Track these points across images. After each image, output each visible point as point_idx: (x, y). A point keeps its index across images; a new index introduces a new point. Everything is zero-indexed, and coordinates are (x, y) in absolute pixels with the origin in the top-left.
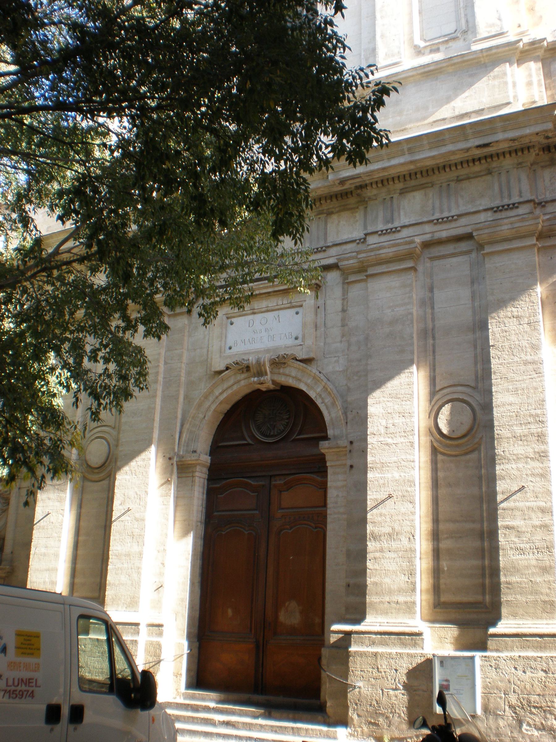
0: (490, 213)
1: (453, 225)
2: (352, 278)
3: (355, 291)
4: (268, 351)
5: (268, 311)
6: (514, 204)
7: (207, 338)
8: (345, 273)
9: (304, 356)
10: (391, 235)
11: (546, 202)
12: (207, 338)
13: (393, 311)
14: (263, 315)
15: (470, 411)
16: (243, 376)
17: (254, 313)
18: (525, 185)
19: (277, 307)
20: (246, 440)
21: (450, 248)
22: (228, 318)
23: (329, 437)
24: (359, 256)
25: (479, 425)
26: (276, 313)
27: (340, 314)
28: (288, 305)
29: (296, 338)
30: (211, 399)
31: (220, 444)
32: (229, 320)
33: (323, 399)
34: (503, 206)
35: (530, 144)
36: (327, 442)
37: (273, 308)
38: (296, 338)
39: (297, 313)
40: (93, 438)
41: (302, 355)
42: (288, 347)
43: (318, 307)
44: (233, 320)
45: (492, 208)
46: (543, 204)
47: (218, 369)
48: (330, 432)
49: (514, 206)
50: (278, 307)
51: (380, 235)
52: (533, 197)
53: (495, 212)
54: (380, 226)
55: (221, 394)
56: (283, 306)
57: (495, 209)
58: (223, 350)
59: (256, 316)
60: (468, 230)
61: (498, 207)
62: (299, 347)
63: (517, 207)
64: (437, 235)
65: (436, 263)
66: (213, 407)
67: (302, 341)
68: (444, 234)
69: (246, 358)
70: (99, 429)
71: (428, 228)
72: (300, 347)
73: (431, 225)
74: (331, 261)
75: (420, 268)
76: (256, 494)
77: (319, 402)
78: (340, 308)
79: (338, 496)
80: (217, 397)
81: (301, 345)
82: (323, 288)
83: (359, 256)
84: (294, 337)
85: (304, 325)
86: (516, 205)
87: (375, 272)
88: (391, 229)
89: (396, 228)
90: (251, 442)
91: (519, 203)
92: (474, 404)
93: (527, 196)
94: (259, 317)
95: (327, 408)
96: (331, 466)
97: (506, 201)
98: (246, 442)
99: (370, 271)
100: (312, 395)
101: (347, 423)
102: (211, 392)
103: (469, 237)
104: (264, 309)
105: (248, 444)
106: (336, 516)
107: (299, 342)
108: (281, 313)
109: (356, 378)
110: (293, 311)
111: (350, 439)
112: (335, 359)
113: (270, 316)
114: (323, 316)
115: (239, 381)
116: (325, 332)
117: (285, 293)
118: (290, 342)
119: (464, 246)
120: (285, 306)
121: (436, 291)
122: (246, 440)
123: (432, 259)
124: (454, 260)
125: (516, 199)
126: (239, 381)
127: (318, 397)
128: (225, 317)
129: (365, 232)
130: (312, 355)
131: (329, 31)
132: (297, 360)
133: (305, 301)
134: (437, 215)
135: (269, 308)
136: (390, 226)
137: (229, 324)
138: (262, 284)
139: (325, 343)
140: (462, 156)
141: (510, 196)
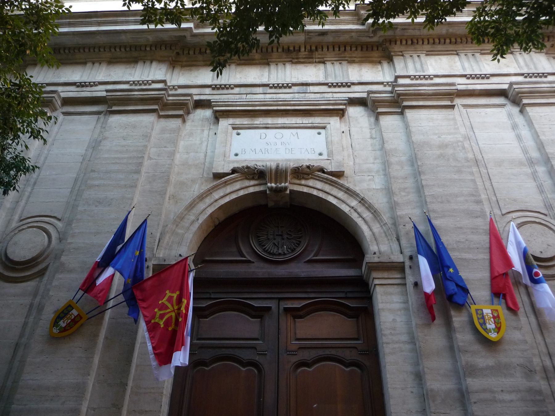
1: (485, 81)
7: (204, 144)
12: (204, 144)
13: (439, 137)
16: (252, 182)
20: (245, 257)
22: (234, 128)
29: (320, 154)
30: (208, 201)
31: (207, 258)
35: (551, 34)
39: (319, 134)
40: (35, 224)
43: (343, 132)
44: (239, 131)
47: (221, 171)
55: (222, 197)
58: (227, 155)
62: (327, 161)
66: (210, 211)
72: (329, 161)
78: (368, 135)
79: (394, 320)
80: (216, 201)
90: (249, 258)
102: (209, 192)
105: (249, 262)
106: (396, 346)
109: (403, 194)
110: (316, 131)
112: (370, 177)
117: (305, 114)
122: (245, 257)
123: (465, 106)
127: (352, 211)
131: (61, 12)
140: (212, 185)
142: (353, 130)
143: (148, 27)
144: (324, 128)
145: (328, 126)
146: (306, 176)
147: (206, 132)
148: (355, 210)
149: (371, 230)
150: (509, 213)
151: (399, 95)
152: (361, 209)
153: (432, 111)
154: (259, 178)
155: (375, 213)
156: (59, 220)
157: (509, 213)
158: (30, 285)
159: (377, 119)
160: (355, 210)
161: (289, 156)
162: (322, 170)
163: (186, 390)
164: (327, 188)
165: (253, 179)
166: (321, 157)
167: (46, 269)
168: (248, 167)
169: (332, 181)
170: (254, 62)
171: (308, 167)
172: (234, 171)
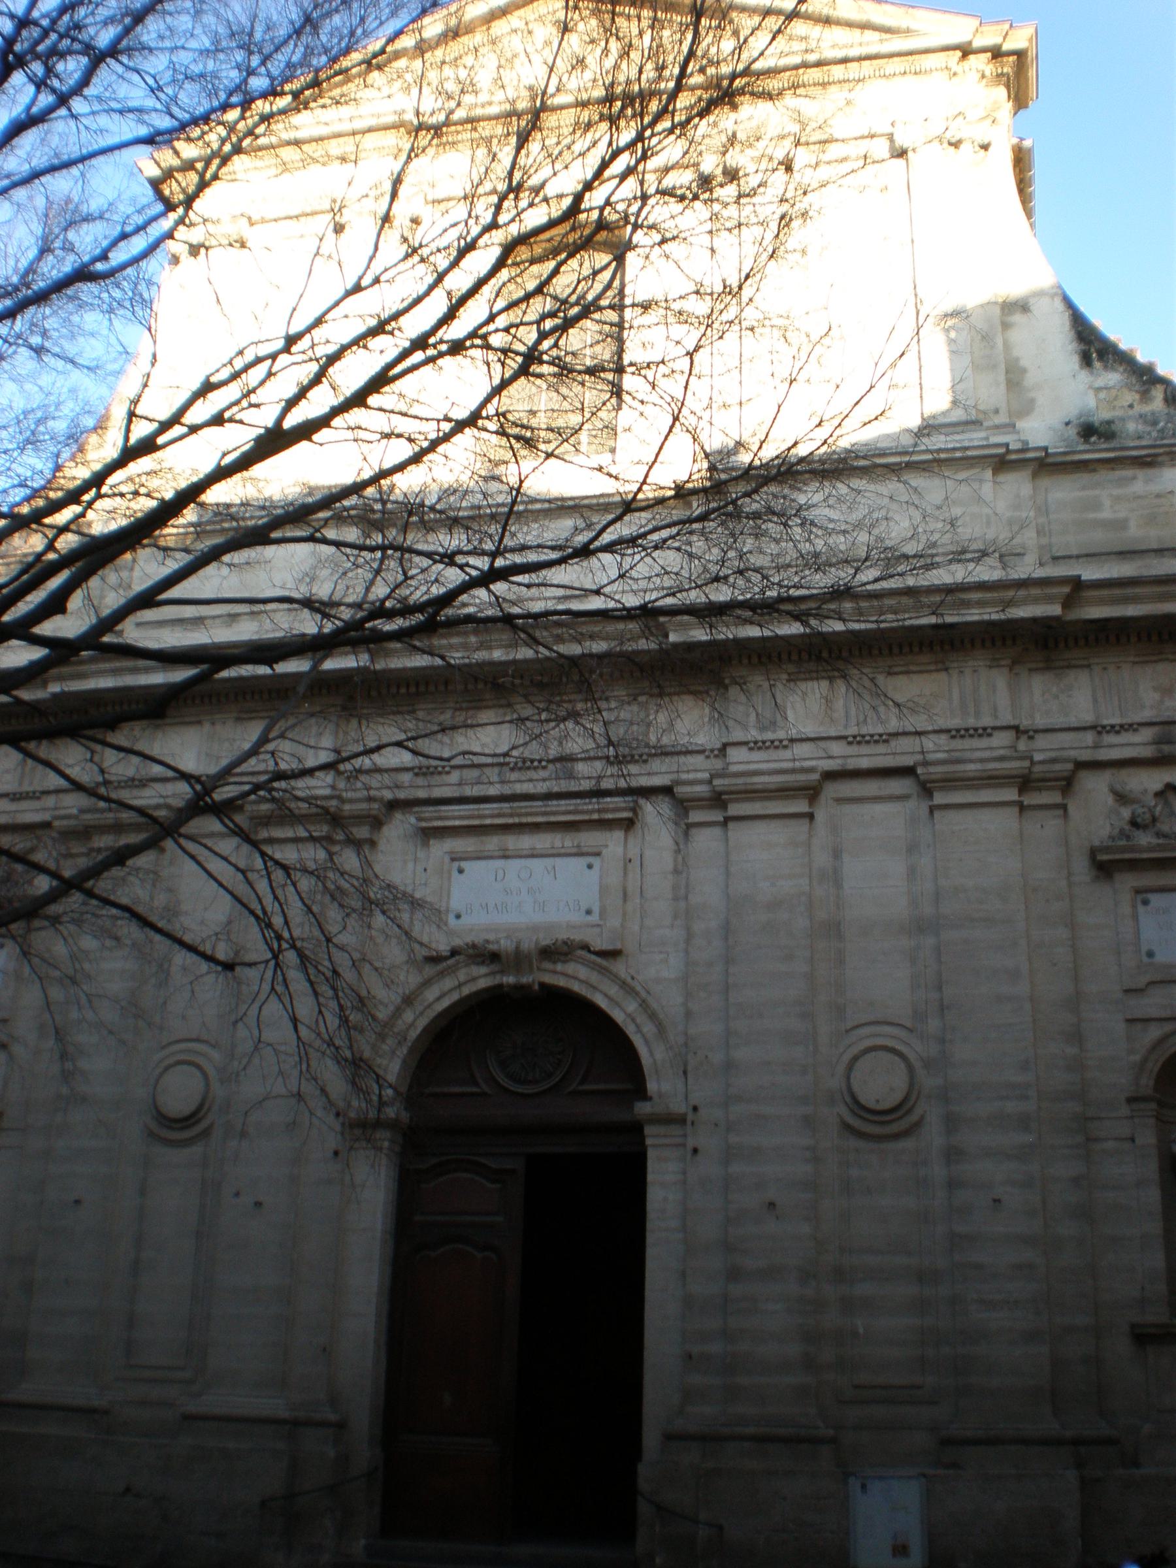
0: (943, 738)
2: (695, 816)
3: (706, 841)
4: (535, 928)
5: (533, 856)
6: (985, 729)
8: (683, 806)
9: (606, 946)
10: (771, 751)
11: (1036, 731)
14: (523, 862)
15: (903, 1065)
16: (483, 970)
17: (506, 857)
18: (1003, 697)
19: (550, 852)
21: (871, 787)
22: (453, 860)
23: (649, 1093)
24: (716, 782)
25: (919, 1093)
26: (549, 862)
27: (670, 877)
28: (574, 850)
29: (589, 912)
32: (456, 864)
33: (637, 1026)
34: (967, 730)
36: (648, 1104)
37: (544, 852)
38: (589, 912)
39: (590, 867)
40: (171, 1060)
41: (599, 944)
42: (574, 927)
44: (464, 864)
45: (949, 731)
46: (1031, 733)
48: (652, 1086)
49: (985, 732)
50: (554, 851)
51: (751, 749)
52: (1016, 722)
53: (953, 737)
54: (754, 734)
55: (438, 999)
56: (563, 851)
57: (954, 733)
59: (510, 862)
60: (908, 761)
61: (958, 731)
63: (990, 735)
64: (852, 764)
65: (848, 809)
67: (601, 919)
68: (865, 763)
69: (491, 937)
70: (183, 1046)
71: (837, 748)
72: (597, 930)
73: (843, 743)
74: (657, 781)
75: (820, 816)
76: (498, 1186)
77: (630, 1030)
78: (671, 867)
81: (598, 925)
82: (638, 825)
83: (716, 782)
84: (583, 909)
85: (604, 890)
86: (989, 731)
87: (742, 813)
88: (772, 742)
89: (781, 741)
90: (486, 1089)
91: (994, 728)
92: (912, 1056)
93: (1006, 718)
94: (514, 865)
95: (646, 1041)
96: (654, 1146)
97: (971, 722)
98: (475, 1089)
99: (734, 809)
100: (618, 1016)
101: (685, 1073)
103: (907, 772)
104: (525, 852)
107: (594, 918)
108: (558, 861)
110: (583, 862)
111: (692, 1102)
112: (662, 956)
113: (537, 864)
114: (639, 876)
115: (474, 979)
116: (642, 907)
118: (577, 918)
119: (896, 786)
120: (569, 851)
121: (846, 858)
123: (840, 801)
124: (878, 808)
125: (987, 721)
126: (474, 979)
127: (629, 1020)
128: (447, 859)
129: (724, 740)
130: (618, 946)
132: (589, 951)
133: (607, 846)
134: (853, 730)
135: (535, 852)
136: (769, 736)
137: (455, 873)
138: (526, 807)
139: (641, 927)
141: (977, 714)
142: (648, 853)
143: (273, 669)
144: (598, 854)
145: (604, 851)
146: (562, 958)
147: (410, 865)
148: (633, 1020)
149: (651, 1054)
150: (857, 1027)
151: (720, 794)
152: (641, 1019)
153: (774, 825)
154: (492, 961)
155: (661, 1029)
156: (213, 1046)
157: (857, 1027)
158: (197, 1150)
159: (686, 834)
160: (633, 1020)
161: (538, 918)
162: (586, 947)
163: (520, 1090)
164: (594, 977)
165: (483, 963)
166: (589, 918)
167: (211, 1127)
168: (474, 946)
169: (600, 966)
170: (485, 703)
171: (565, 943)
172: (454, 952)
